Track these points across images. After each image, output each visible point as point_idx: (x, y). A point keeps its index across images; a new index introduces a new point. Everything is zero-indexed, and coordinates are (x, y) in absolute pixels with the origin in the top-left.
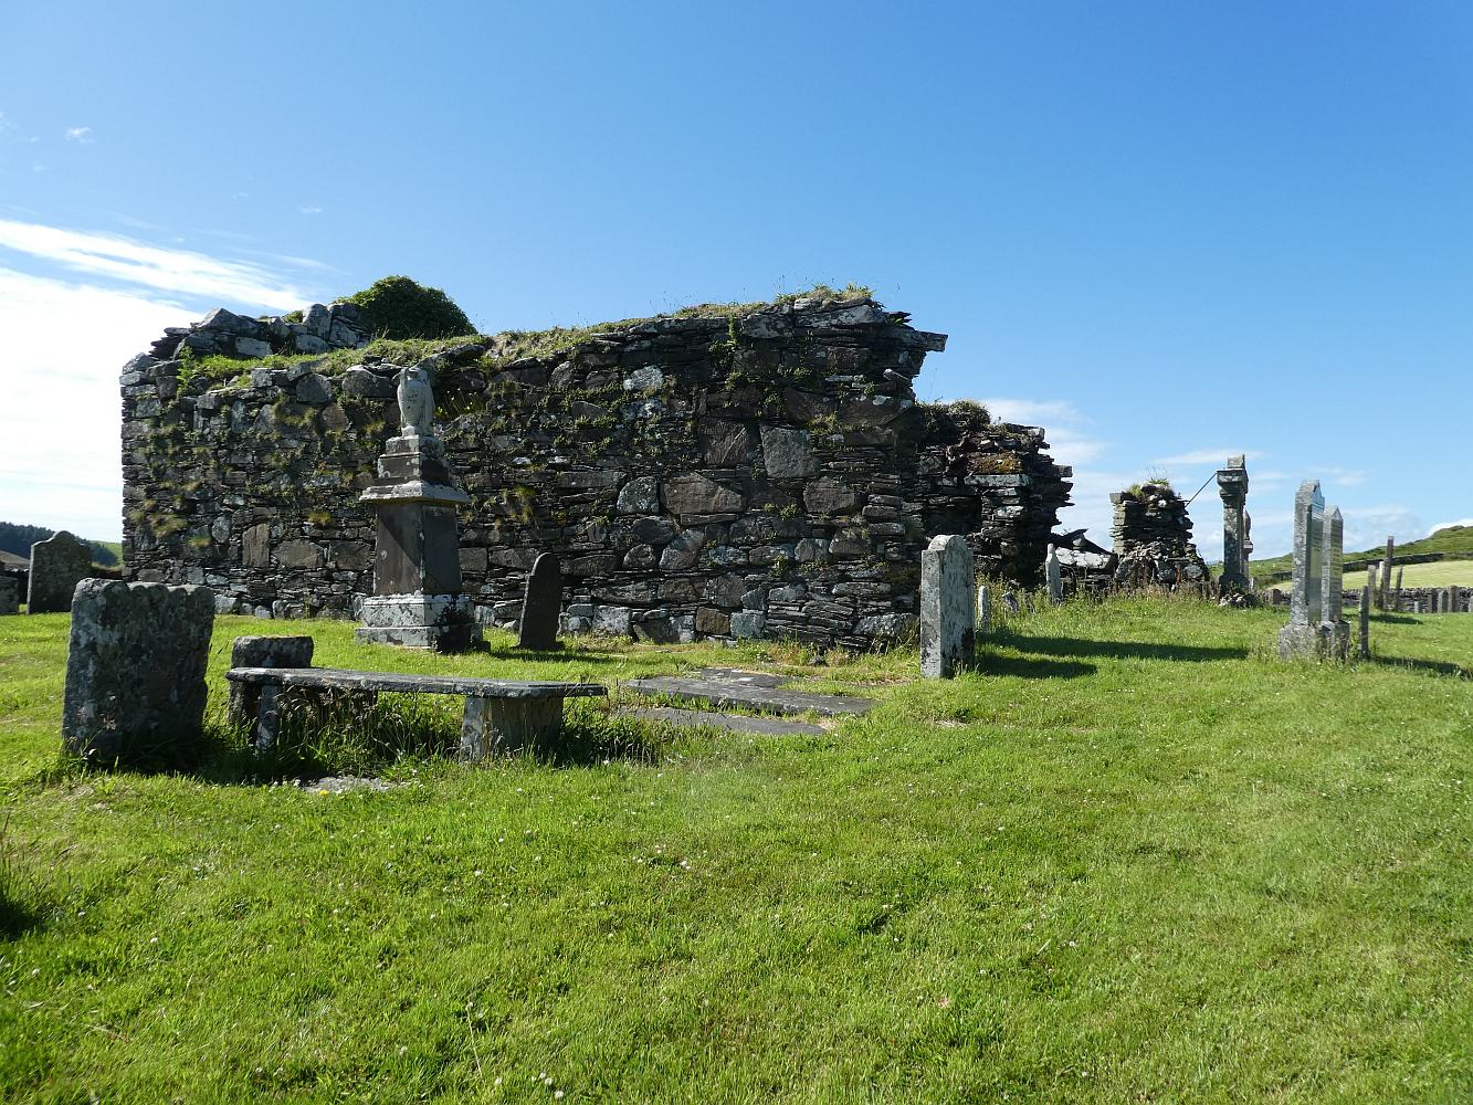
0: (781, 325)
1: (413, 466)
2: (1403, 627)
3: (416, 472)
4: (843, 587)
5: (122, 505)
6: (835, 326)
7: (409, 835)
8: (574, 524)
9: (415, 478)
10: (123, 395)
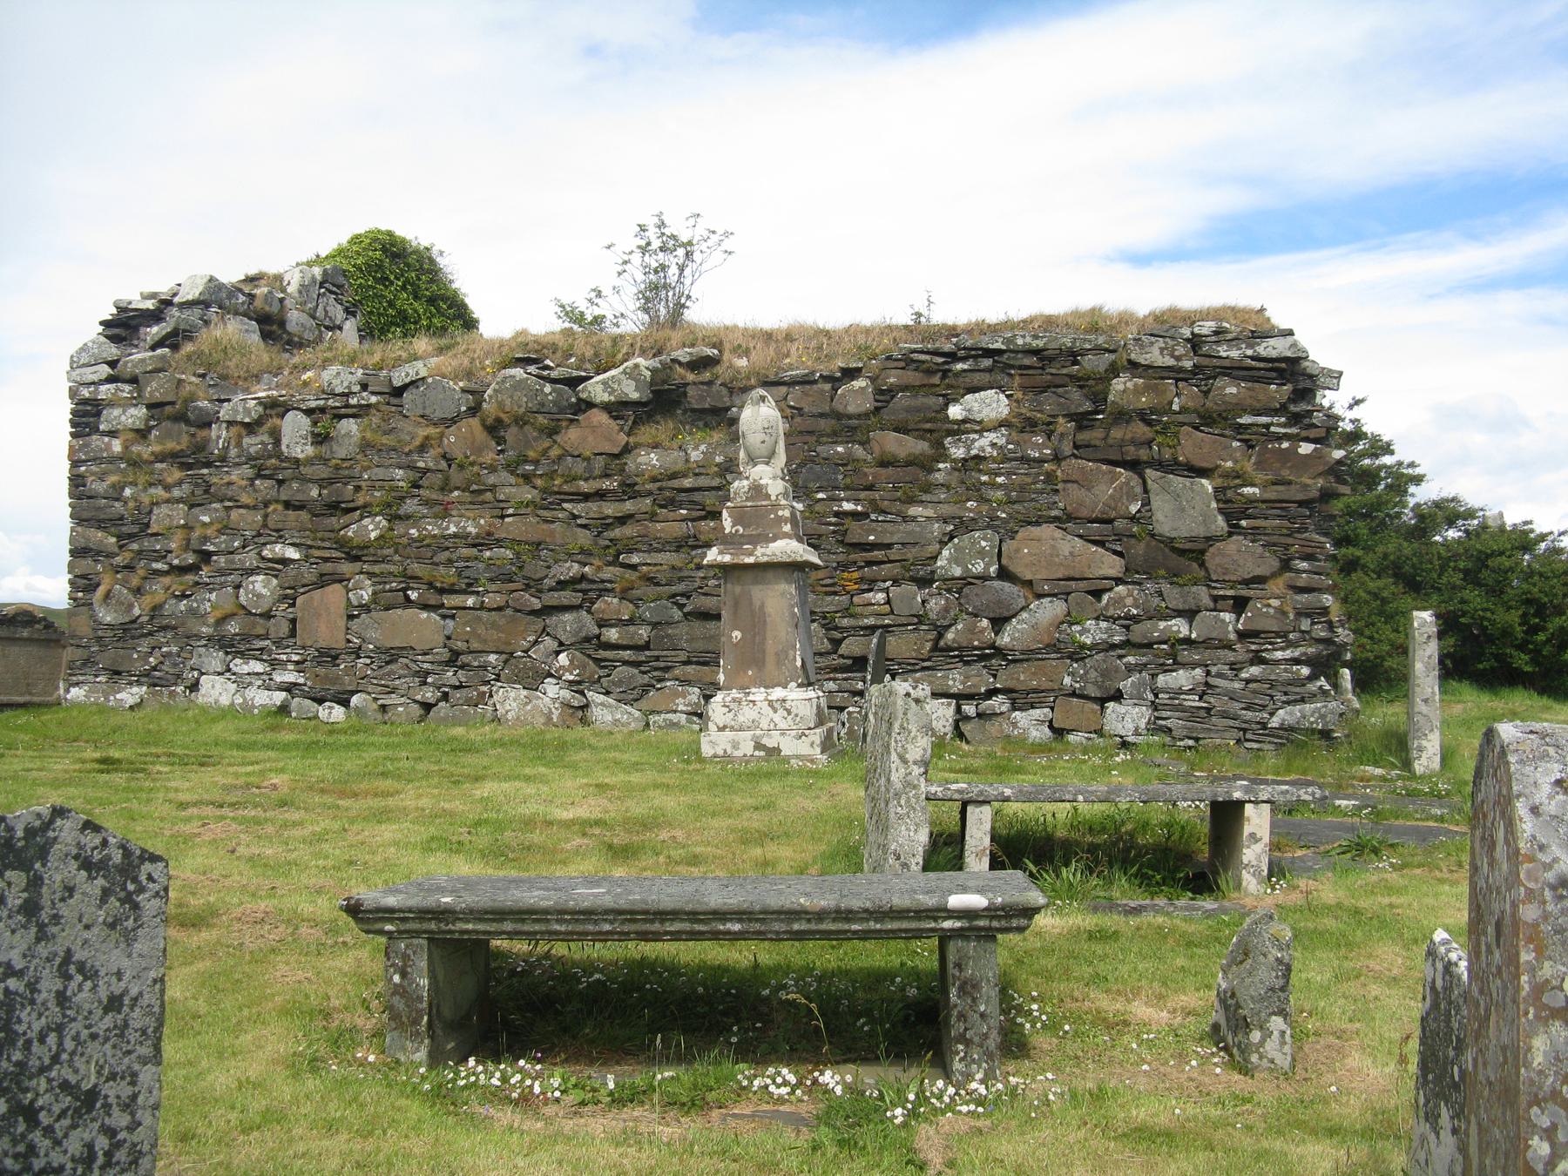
0: (1180, 351)
1: (780, 520)
2: (23, 718)
3: (787, 528)
4: (1255, 670)
5: (68, 558)
6: (1252, 358)
7: (1542, 848)
8: (870, 590)
9: (786, 536)
10: (71, 397)
